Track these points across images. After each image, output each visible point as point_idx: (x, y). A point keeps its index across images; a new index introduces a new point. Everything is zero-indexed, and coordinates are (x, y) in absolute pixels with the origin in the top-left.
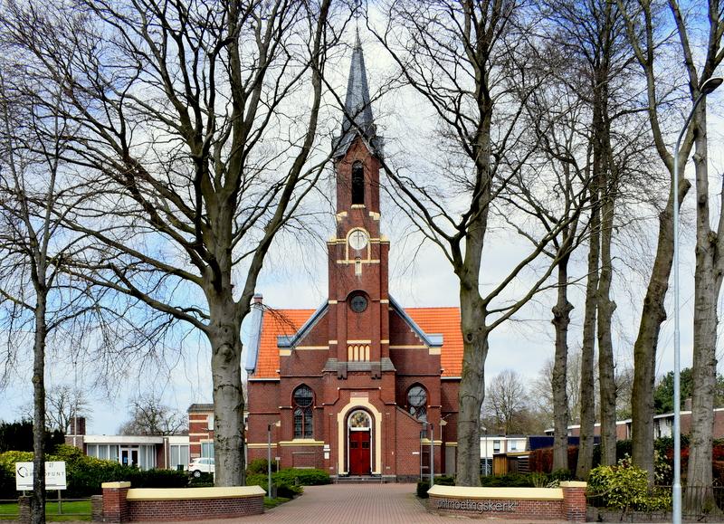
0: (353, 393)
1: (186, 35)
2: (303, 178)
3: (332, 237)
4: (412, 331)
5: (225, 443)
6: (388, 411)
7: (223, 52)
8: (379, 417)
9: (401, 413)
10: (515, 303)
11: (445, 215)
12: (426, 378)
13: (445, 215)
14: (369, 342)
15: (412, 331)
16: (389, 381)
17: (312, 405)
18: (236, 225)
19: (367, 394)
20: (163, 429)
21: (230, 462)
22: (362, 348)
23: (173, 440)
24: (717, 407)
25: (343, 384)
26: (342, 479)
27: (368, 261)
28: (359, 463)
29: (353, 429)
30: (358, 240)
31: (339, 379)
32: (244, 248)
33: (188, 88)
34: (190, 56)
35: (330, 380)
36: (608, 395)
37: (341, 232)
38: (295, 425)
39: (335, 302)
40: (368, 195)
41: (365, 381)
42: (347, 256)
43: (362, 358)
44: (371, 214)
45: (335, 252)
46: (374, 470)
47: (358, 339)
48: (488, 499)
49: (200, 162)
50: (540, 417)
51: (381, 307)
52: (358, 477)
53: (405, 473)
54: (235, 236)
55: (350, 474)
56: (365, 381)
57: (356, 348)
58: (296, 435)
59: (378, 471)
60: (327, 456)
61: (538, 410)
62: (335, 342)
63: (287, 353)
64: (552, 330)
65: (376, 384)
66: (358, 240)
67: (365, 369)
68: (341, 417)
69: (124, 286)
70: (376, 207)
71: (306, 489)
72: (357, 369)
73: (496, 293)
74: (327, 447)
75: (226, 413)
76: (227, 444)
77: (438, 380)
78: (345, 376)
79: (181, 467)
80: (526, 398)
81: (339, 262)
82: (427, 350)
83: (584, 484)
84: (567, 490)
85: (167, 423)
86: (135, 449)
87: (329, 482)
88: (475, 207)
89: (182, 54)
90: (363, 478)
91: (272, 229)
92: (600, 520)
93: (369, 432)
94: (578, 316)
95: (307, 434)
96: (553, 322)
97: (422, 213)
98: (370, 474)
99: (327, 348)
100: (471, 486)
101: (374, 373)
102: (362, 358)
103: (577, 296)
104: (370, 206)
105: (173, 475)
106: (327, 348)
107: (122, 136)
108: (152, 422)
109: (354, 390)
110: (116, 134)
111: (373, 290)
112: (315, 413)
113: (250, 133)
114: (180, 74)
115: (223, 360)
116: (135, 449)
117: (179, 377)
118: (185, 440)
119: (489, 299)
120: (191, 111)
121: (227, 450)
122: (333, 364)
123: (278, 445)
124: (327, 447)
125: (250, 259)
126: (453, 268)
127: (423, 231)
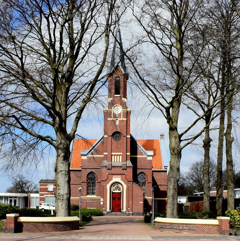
1: (51, 16)
2: (99, 80)
4: (140, 149)
5: (62, 197)
7: (67, 25)
8: (125, 186)
9: (135, 185)
10: (192, 137)
11: (163, 98)
12: (146, 170)
13: (163, 98)
14: (121, 154)
15: (140, 149)
16: (130, 171)
17: (95, 181)
18: (69, 101)
19: (120, 176)
20: (26, 190)
21: (64, 206)
23: (32, 195)
24: (82, 196)
25: (109, 172)
27: (121, 119)
28: (116, 205)
30: (118, 110)
31: (108, 169)
32: (72, 110)
33: (51, 40)
34: (52, 26)
35: (104, 170)
36: (231, 178)
37: (112, 104)
38: (87, 190)
39: (107, 136)
40: (122, 90)
41: (120, 171)
42: (112, 116)
45: (107, 114)
46: (123, 210)
47: (116, 152)
49: (56, 71)
50: (190, 188)
52: (116, 213)
53: (136, 211)
54: (69, 104)
55: (112, 212)
56: (120, 171)
57: (116, 156)
58: (88, 194)
59: (125, 210)
60: (102, 203)
61: (189, 185)
62: (106, 153)
64: (203, 150)
65: (124, 172)
67: (120, 165)
68: (108, 186)
69: (18, 125)
70: (125, 96)
71: (94, 217)
73: (186, 132)
75: (62, 183)
77: (151, 170)
78: (110, 168)
79: (38, 207)
80: (184, 179)
81: (109, 119)
83: (229, 218)
84: (220, 221)
85: (28, 188)
86: (15, 199)
87: (102, 214)
88: (177, 95)
89: (49, 26)
90: (118, 213)
91: (86, 102)
92: (236, 235)
94: (214, 144)
95: (93, 193)
96: (203, 147)
97: (154, 96)
98: (121, 211)
99: (103, 156)
100: (174, 218)
101: (123, 167)
103: (214, 135)
104: (122, 95)
105: (35, 210)
106: (103, 156)
107: (21, 59)
108: (22, 187)
110: (19, 58)
112: (97, 184)
113: (77, 60)
114: (47, 34)
116: (15, 199)
117: (41, 167)
118: (37, 195)
119: (182, 135)
120: (52, 52)
121: (63, 200)
122: (106, 163)
124: (102, 199)
125: (76, 114)
126: (166, 121)
127: (153, 104)
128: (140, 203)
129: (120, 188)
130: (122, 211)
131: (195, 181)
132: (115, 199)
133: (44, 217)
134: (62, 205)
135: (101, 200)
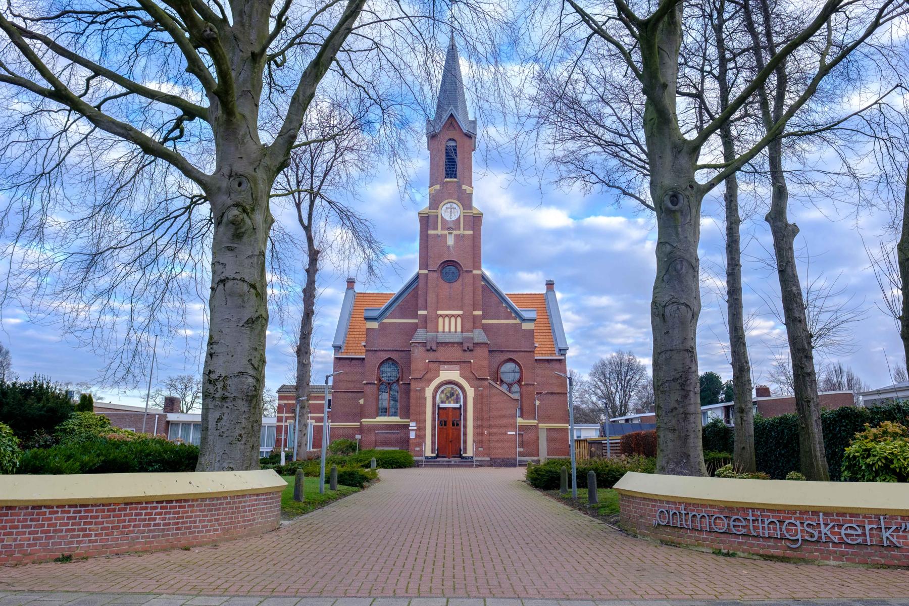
0: (442, 366)
3: (425, 205)
5: (220, 385)
6: (481, 386)
8: (470, 392)
12: (519, 353)
14: (460, 312)
19: (458, 367)
22: (453, 320)
25: (432, 356)
26: (430, 463)
27: (462, 232)
29: (442, 405)
37: (435, 202)
41: (456, 353)
43: (453, 330)
44: (464, 187)
45: (426, 221)
46: (465, 451)
48: (815, 512)
51: (474, 278)
52: (447, 459)
53: (499, 456)
55: (437, 456)
56: (456, 353)
57: (447, 320)
60: (412, 435)
63: (375, 325)
65: (467, 356)
66: (450, 212)
67: (457, 340)
71: (382, 473)
72: (447, 341)
74: (413, 425)
76: (224, 387)
78: (434, 348)
82: (520, 325)
93: (460, 409)
98: (461, 456)
102: (453, 330)
106: (416, 321)
109: (444, 363)
111: (465, 264)
115: (230, 233)
121: (224, 398)
122: (421, 335)
123: (361, 424)
128: (509, 433)
129: (457, 395)
130: (464, 455)
131: (600, 398)
132: (445, 425)
133: (55, 473)
134: (219, 420)
135: (410, 428)
